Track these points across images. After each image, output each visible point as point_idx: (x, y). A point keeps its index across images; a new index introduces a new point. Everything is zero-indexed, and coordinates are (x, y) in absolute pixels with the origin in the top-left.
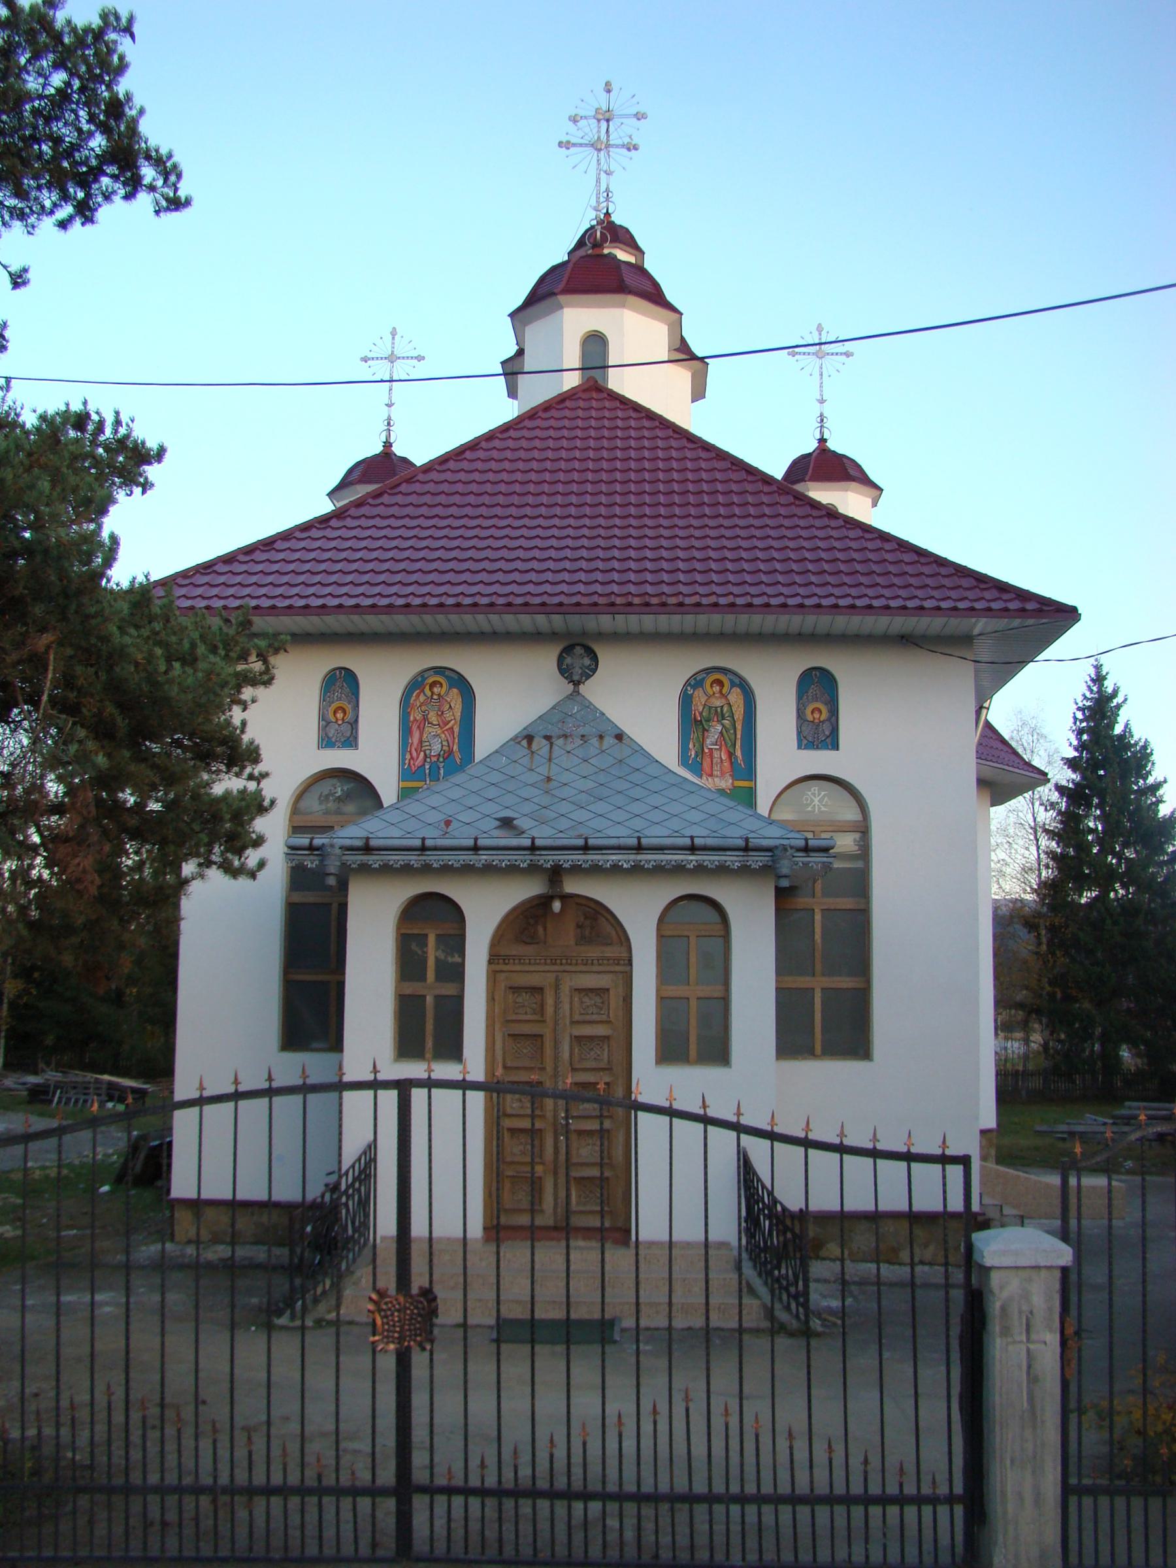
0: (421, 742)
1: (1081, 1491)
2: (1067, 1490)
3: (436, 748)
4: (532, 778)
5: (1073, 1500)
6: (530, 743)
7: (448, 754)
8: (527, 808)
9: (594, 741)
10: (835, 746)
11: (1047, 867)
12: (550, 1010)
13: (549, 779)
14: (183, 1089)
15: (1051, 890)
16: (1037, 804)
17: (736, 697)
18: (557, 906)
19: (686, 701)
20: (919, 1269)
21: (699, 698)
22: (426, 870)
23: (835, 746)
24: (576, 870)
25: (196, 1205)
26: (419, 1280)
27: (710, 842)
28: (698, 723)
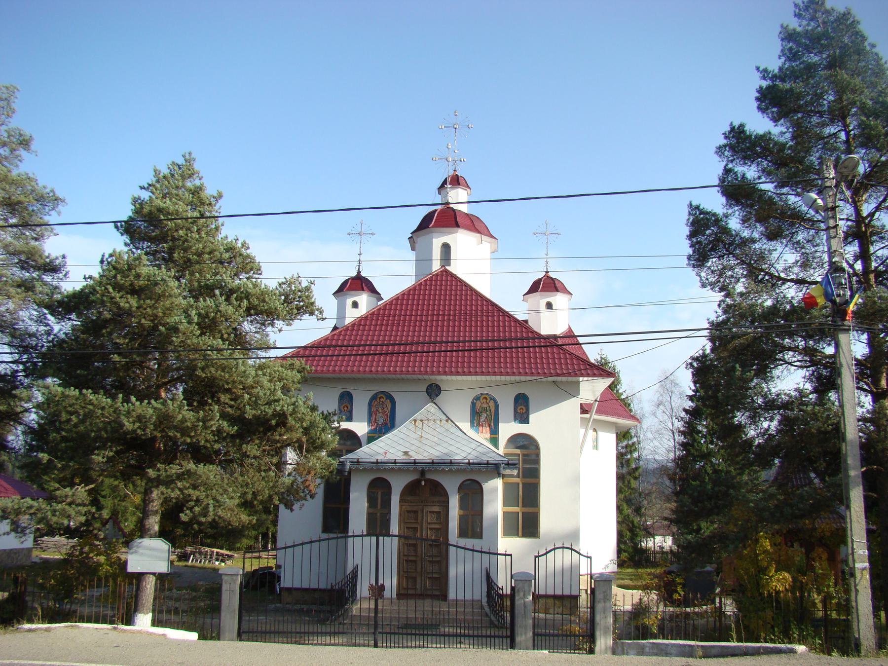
0: (376, 419)
1: (538, 635)
2: (534, 634)
3: (381, 421)
4: (416, 436)
5: (536, 637)
6: (415, 422)
7: (385, 424)
8: (413, 448)
9: (438, 422)
10: (528, 422)
11: (679, 449)
12: (420, 518)
13: (422, 437)
14: (350, 533)
15: (680, 462)
16: (674, 418)
17: (492, 404)
18: (423, 483)
19: (473, 405)
20: (556, 616)
21: (478, 404)
22: (378, 470)
23: (528, 422)
24: (429, 470)
25: (289, 590)
26: (380, 582)
27: (475, 461)
28: (478, 413)
